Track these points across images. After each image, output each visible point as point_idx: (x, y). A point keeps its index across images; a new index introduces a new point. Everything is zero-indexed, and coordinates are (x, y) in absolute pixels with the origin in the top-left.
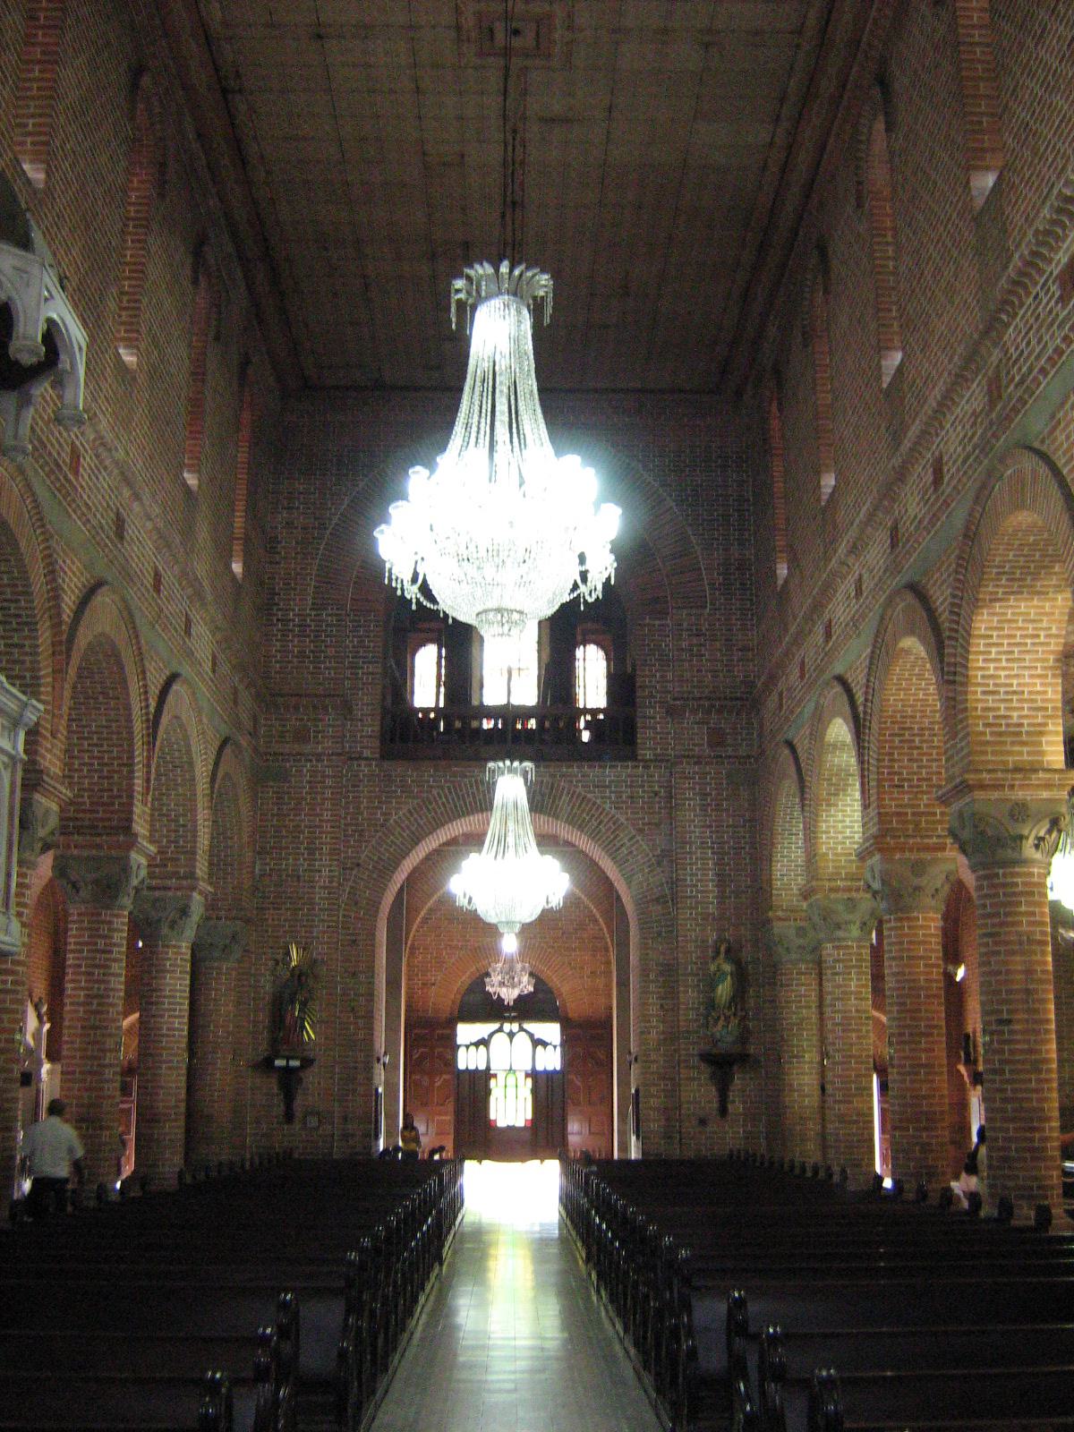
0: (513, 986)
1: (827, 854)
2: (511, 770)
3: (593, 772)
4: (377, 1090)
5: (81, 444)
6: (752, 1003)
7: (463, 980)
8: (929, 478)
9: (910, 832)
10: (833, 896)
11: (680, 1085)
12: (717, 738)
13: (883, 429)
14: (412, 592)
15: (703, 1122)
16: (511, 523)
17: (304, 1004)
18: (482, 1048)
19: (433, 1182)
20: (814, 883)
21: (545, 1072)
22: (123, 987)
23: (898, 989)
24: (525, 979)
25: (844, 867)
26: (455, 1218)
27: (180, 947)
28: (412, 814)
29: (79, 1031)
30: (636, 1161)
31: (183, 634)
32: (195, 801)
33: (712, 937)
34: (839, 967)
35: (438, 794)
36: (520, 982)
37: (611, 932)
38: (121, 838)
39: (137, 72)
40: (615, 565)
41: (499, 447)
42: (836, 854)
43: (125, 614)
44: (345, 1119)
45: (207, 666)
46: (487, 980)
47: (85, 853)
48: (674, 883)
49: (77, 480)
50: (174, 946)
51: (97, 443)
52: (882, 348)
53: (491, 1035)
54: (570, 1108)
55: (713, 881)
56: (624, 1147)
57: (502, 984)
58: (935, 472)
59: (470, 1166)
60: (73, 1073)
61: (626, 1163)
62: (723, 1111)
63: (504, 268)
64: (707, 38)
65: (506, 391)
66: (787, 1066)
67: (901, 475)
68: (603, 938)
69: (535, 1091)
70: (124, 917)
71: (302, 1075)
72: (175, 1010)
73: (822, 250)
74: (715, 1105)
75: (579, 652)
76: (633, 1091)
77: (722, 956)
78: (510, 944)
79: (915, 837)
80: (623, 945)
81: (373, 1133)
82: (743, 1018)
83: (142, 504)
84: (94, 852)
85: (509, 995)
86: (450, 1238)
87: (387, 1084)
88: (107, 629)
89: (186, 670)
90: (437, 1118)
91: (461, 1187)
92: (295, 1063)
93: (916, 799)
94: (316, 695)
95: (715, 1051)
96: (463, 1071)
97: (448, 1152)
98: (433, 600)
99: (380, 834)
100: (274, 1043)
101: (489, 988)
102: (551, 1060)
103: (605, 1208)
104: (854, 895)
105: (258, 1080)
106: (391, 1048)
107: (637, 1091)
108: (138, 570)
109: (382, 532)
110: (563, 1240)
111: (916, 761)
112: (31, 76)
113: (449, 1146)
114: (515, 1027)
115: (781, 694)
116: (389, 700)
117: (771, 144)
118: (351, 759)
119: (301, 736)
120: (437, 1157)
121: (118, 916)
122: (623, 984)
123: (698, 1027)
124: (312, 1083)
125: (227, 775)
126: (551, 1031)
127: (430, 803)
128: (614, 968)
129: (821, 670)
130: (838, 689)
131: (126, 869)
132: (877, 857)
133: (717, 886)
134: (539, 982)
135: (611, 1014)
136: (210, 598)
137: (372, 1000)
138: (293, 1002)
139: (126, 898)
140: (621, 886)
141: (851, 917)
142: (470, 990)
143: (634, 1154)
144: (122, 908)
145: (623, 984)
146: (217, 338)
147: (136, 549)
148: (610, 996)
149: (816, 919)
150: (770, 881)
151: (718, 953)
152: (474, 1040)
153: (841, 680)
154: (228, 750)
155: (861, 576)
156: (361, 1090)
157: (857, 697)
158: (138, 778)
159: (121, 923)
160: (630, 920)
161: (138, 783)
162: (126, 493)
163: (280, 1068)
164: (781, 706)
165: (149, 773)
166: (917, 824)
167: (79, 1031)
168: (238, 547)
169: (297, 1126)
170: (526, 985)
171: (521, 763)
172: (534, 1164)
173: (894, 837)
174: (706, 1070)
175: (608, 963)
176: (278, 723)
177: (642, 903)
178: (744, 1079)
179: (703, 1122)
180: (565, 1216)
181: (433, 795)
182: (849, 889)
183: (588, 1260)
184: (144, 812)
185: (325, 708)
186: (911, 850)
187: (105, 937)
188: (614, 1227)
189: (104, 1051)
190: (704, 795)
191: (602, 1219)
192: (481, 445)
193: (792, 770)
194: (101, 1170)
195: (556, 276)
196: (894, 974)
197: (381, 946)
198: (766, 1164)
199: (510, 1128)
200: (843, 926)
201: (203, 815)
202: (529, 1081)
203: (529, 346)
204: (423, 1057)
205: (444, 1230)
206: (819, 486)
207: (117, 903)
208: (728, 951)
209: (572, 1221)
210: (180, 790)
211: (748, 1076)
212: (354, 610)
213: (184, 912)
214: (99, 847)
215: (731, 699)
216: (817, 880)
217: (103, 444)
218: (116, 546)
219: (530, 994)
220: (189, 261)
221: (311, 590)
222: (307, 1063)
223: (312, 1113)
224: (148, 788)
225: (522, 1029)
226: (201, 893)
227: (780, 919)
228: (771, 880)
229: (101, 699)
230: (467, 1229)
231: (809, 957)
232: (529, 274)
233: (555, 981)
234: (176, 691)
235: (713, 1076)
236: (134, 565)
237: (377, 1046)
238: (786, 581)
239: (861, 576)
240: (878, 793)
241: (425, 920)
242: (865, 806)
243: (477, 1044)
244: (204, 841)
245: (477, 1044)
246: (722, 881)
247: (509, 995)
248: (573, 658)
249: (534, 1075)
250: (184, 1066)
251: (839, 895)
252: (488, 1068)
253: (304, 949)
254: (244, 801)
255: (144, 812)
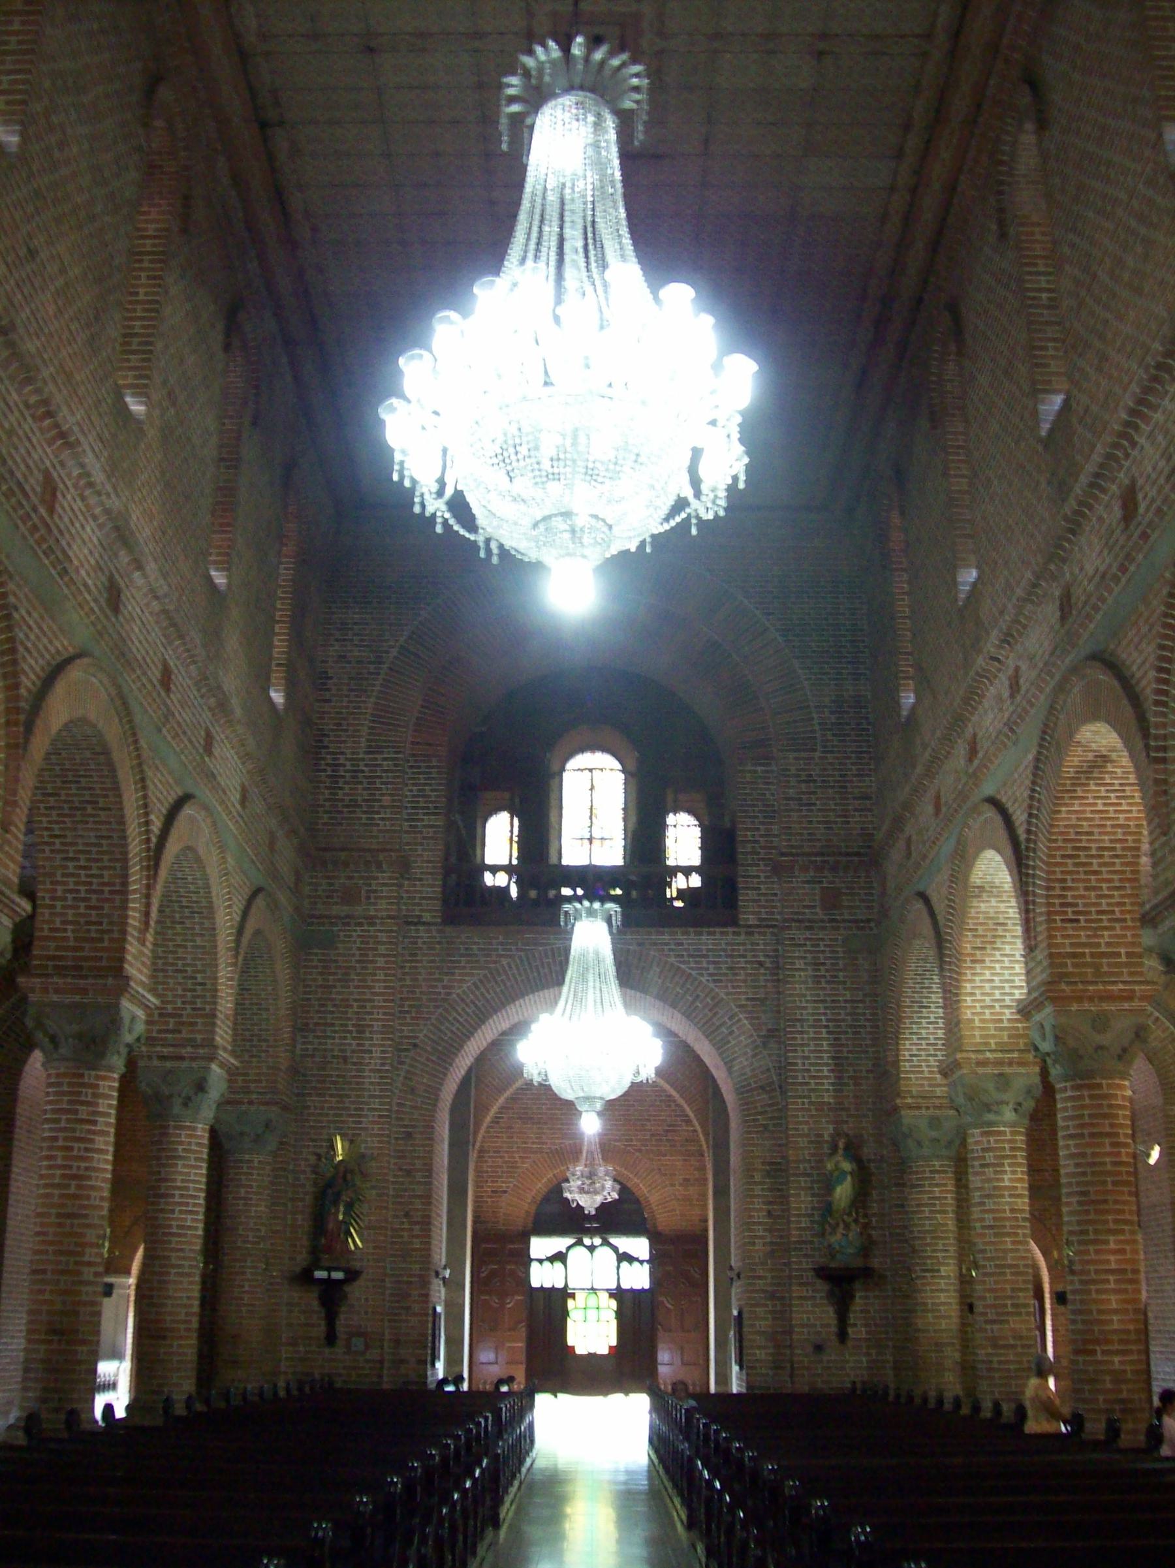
0: (596, 1192)
1: (972, 1021)
2: (591, 913)
3: (689, 939)
4: (435, 1309)
5: (60, 476)
6: (875, 1208)
7: (540, 1186)
8: (1117, 512)
9: (1090, 978)
10: (980, 1070)
11: (790, 1305)
12: (831, 900)
13: (1043, 485)
14: (436, 507)
15: (819, 1348)
16: (588, 367)
17: (349, 1206)
18: (558, 1265)
19: (486, 1420)
20: (959, 1056)
21: (632, 1290)
22: (109, 1167)
23: (1079, 1174)
24: (609, 1184)
25: (993, 1036)
26: (521, 1462)
27: (195, 1129)
28: (477, 988)
29: (53, 1219)
30: (739, 1395)
31: (201, 751)
32: (216, 953)
33: (828, 1131)
34: (990, 1157)
35: (509, 964)
36: (603, 1188)
37: (706, 1134)
38: (110, 981)
39: (154, 82)
40: (746, 460)
41: (569, 272)
42: (983, 1021)
43: (118, 703)
44: (397, 1342)
45: (235, 797)
46: (565, 1185)
47: (68, 999)
48: (783, 1067)
49: (52, 518)
50: (189, 1128)
51: (82, 482)
52: (1038, 390)
53: (569, 1248)
54: (661, 1333)
55: (827, 1064)
56: (723, 1378)
57: (582, 1190)
58: (1125, 506)
59: (542, 1400)
60: (44, 1272)
61: (725, 1397)
62: (842, 1336)
63: (578, 47)
64: (821, 45)
65: (580, 222)
66: (919, 1282)
67: (1074, 526)
68: (699, 1141)
69: (619, 1314)
70: (114, 1080)
71: (347, 1288)
72: (187, 1204)
73: (953, 308)
74: (834, 1329)
75: (671, 819)
76: (735, 1313)
77: (841, 1152)
78: (590, 1125)
79: (1096, 983)
80: (721, 1146)
81: (429, 1358)
82: (866, 1226)
83: (145, 576)
84: (77, 998)
85: (589, 1203)
86: (513, 1490)
87: (448, 1305)
88: (93, 716)
89: (204, 792)
90: (508, 1345)
91: (531, 1426)
92: (338, 1275)
93: (1096, 936)
94: (369, 850)
95: (832, 1265)
96: (537, 1289)
97: (519, 1383)
98: (469, 521)
99: (440, 1010)
100: (314, 1251)
101: (567, 1195)
102: (638, 1278)
103: (721, 1460)
104: (1007, 1070)
105: (295, 1295)
106: (455, 1262)
107: (740, 1313)
108: (139, 657)
109: (392, 409)
110: (654, 1494)
111: (1094, 888)
112: (10, 28)
113: (520, 1374)
114: (597, 1241)
115: (909, 841)
116: (453, 860)
117: (893, 189)
118: (408, 923)
119: (350, 896)
120: (504, 1389)
121: (104, 1078)
122: (721, 1192)
123: (813, 1236)
124: (359, 1299)
125: (258, 933)
126: (639, 1246)
127: (499, 974)
128: (710, 1176)
129: (963, 796)
130: (990, 813)
131: (114, 1023)
132: (1049, 1009)
133: (832, 1071)
134: (624, 1190)
135: (706, 1230)
136: (238, 713)
137: (430, 1204)
138: (336, 1203)
139: (115, 1057)
140: (720, 1074)
141: (1005, 1097)
142: (546, 1199)
143: (736, 1386)
144: (111, 1069)
145: (721, 1192)
146: (254, 423)
147: (137, 630)
148: (705, 1207)
149: (961, 1100)
150: (896, 1063)
151: (834, 1149)
152: (549, 1255)
153: (993, 802)
154: (260, 901)
155: (1017, 669)
156: (416, 1308)
157: (1014, 817)
158: (134, 909)
159: (110, 1086)
160: (731, 1115)
161: (134, 918)
162: (124, 558)
163: (321, 1281)
164: (909, 855)
165: (148, 905)
166: (1097, 967)
167: (53, 1219)
168: (277, 676)
169: (339, 1349)
170: (609, 1192)
171: (602, 905)
172: (617, 1398)
173: (1069, 983)
174: (822, 1286)
175: (703, 1168)
176: (324, 881)
177: (743, 1091)
178: (867, 1298)
179: (819, 1348)
180: (656, 1461)
181: (503, 966)
182: (999, 1063)
183: (690, 1525)
184: (141, 953)
185: (379, 866)
186: (1091, 999)
187: (88, 1103)
188: (737, 1486)
189: (83, 1245)
190: (817, 965)
191: (715, 1474)
192: (544, 258)
193: (926, 927)
194: (75, 1396)
195: (655, 74)
196: (1072, 1156)
197: (442, 1141)
198: (903, 1400)
199: (591, 1356)
200: (995, 1108)
201: (226, 975)
202: (614, 1304)
203: (615, 170)
204: (493, 1274)
205: (503, 1481)
206: (955, 583)
207: (104, 1063)
208: (846, 1148)
209: (672, 1479)
210: (199, 941)
211: (870, 1294)
212: (414, 755)
213: (201, 1087)
214: (84, 991)
215: (848, 854)
216: (962, 1051)
217: (91, 485)
218: (107, 617)
219: (615, 1201)
220: (220, 326)
221: (365, 731)
222: (353, 1275)
223: (360, 1334)
224: (147, 924)
225: (606, 1243)
226: (222, 1065)
227: (910, 1107)
228: (898, 1061)
229: (89, 811)
230: (538, 1477)
231: (944, 1152)
232: (615, 62)
233: (642, 1187)
234: (192, 820)
235: (831, 1294)
236: (134, 650)
237: (436, 1257)
238: (914, 708)
239: (1017, 669)
240: (1049, 929)
241: (496, 1121)
242: (1030, 948)
243: (552, 1259)
244: (226, 1003)
245: (552, 1259)
246: (839, 1064)
247: (589, 1203)
248: (663, 826)
249: (618, 1294)
250: (198, 1272)
251: (989, 1070)
252: (566, 1285)
253: (351, 1142)
254: (283, 971)
255: (141, 953)
